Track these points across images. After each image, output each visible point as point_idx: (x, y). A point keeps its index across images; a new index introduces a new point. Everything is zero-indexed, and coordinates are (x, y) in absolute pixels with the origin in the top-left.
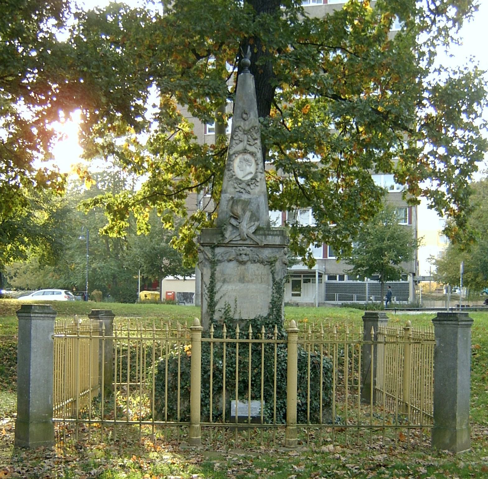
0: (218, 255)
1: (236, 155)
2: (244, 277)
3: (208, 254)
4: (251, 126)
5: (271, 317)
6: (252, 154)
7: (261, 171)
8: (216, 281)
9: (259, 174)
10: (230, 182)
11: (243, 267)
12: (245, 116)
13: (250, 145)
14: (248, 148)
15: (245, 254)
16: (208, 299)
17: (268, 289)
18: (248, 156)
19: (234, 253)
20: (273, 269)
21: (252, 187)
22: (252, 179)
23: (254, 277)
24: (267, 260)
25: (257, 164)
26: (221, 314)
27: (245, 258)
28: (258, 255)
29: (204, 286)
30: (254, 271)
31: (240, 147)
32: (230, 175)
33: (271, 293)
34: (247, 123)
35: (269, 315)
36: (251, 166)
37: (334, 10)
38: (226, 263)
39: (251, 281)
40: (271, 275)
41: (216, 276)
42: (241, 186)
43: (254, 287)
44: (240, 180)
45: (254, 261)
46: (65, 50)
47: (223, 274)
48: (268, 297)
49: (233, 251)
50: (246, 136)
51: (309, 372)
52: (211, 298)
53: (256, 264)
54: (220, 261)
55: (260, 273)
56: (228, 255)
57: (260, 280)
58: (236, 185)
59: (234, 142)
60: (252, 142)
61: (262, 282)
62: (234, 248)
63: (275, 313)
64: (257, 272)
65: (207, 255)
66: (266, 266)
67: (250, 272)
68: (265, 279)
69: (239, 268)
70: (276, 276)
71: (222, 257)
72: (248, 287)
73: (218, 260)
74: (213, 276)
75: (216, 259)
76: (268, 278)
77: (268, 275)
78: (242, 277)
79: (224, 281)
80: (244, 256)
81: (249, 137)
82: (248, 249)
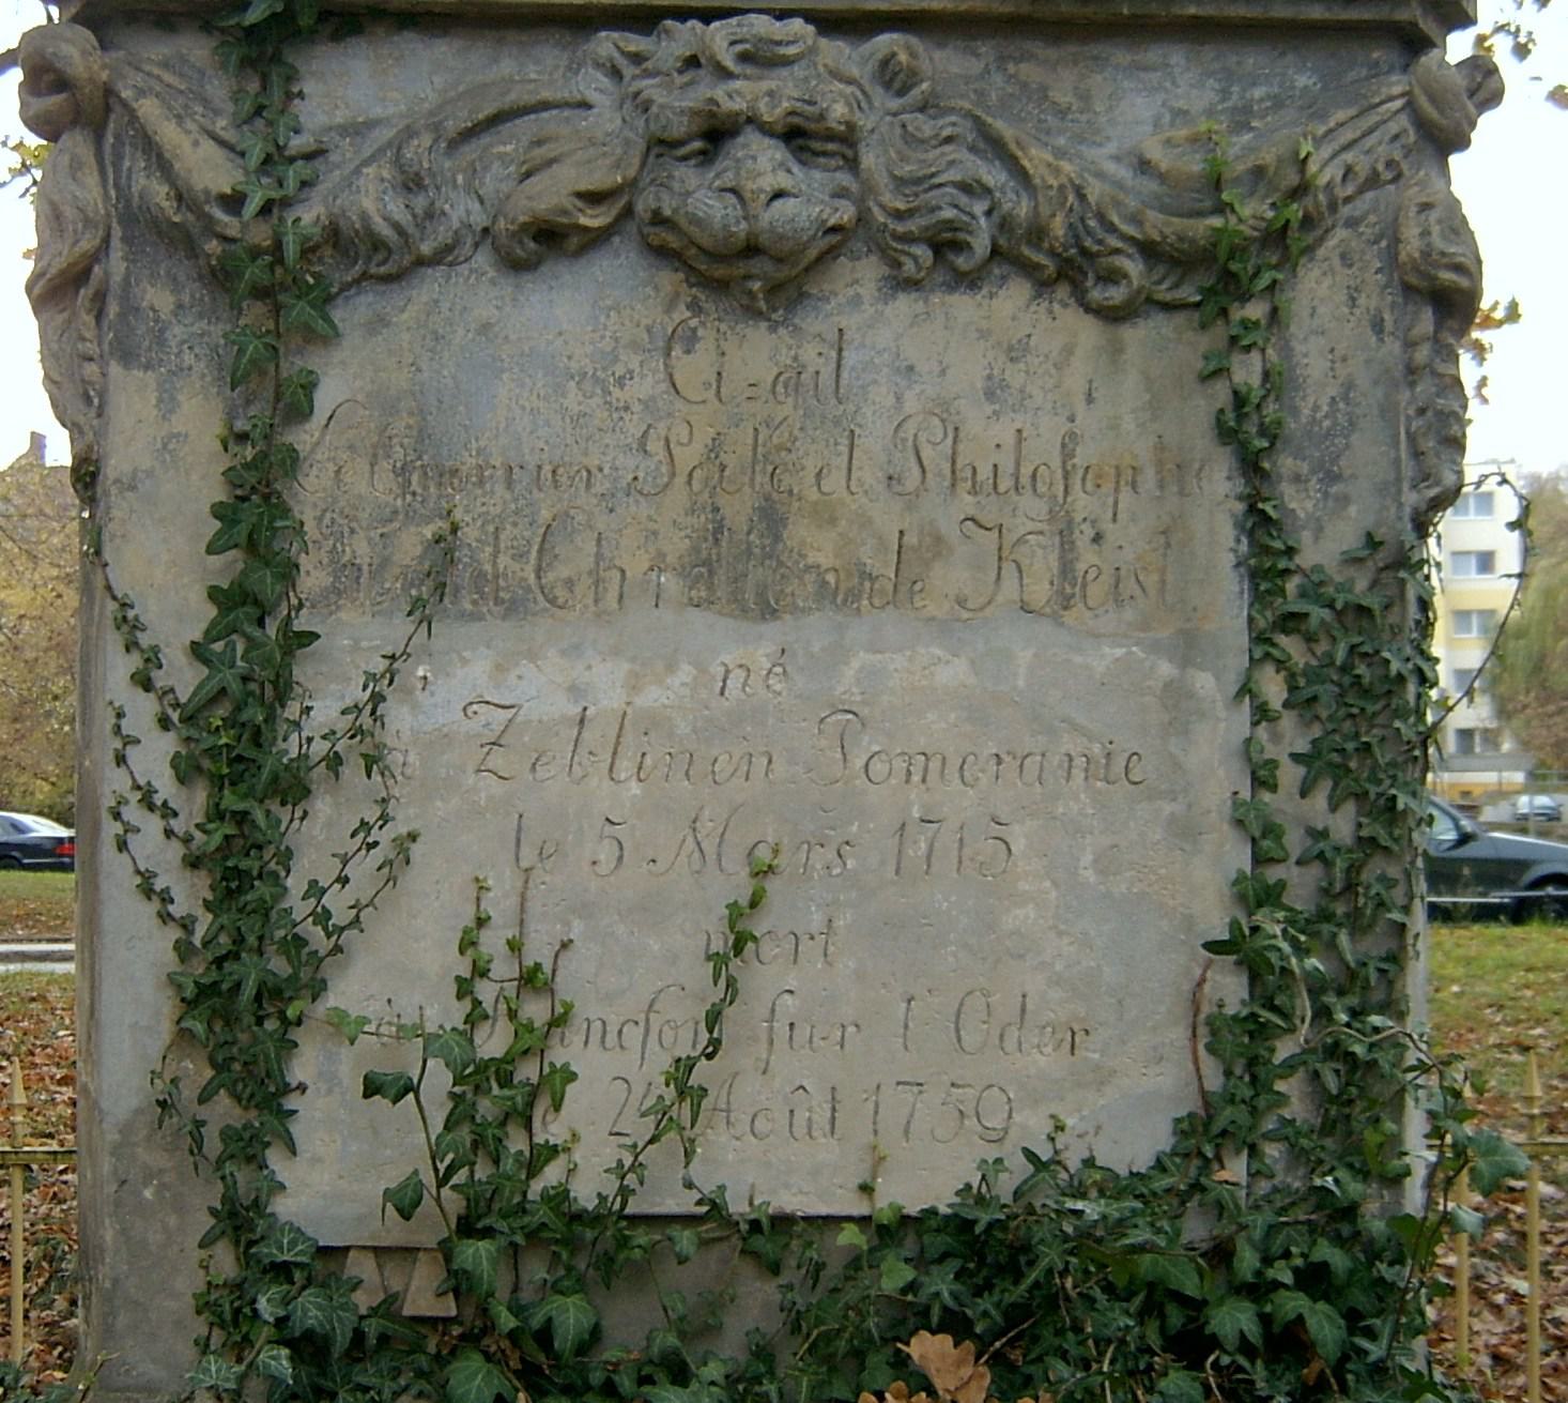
0: (344, 152)
2: (771, 518)
3: (169, 134)
5: (1236, 1169)
8: (313, 578)
11: (756, 352)
15: (798, 137)
16: (189, 893)
17: (1176, 696)
19: (607, 117)
20: (1247, 372)
23: (947, 514)
24: (1157, 225)
26: (405, 1142)
27: (789, 196)
28: (995, 147)
29: (119, 667)
30: (942, 409)
33: (1217, 780)
35: (1202, 1135)
37: (1091, 1150)
38: (474, 295)
39: (893, 582)
40: (1220, 484)
41: (309, 496)
43: (953, 672)
45: (945, 243)
46: (930, 233)
47: (425, 464)
48: (1185, 831)
49: (592, 84)
52: (239, 867)
53: (964, 306)
54: (376, 260)
55: (1044, 448)
56: (508, 144)
57: (1042, 563)
61: (1069, 588)
62: (606, 43)
63: (1295, 1100)
64: (988, 436)
65: (162, 165)
66: (1135, 335)
67: (874, 437)
68: (1130, 538)
69: (694, 367)
70: (1296, 500)
71: (411, 183)
72: (846, 682)
73: (335, 236)
74: (255, 512)
75: (310, 215)
76: (1169, 535)
77: (1177, 472)
78: (739, 509)
79: (439, 587)
80: (762, 162)
82: (836, 51)
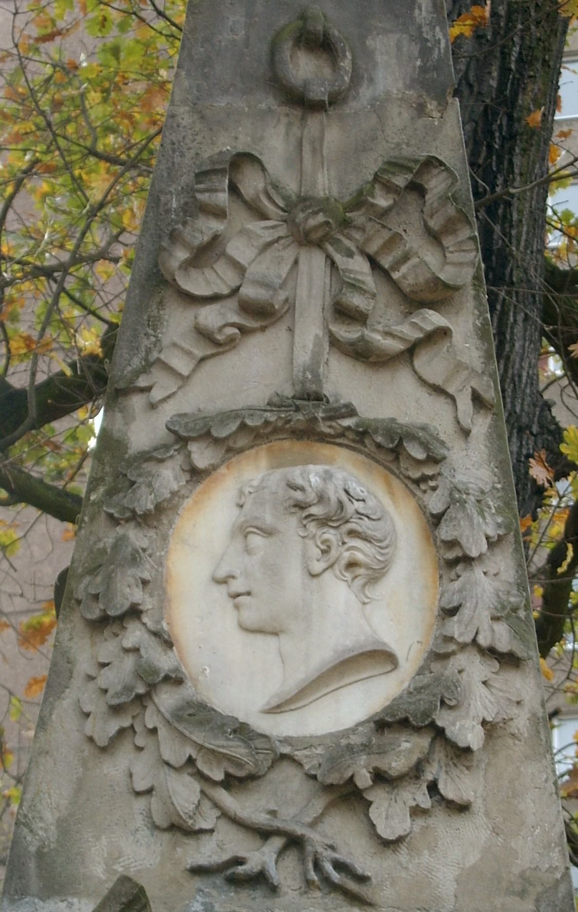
1: (202, 456)
4: (372, 164)
6: (393, 449)
7: (502, 637)
9: (474, 670)
10: (115, 768)
12: (304, 68)
13: (363, 355)
14: (345, 382)
18: (339, 473)
21: (390, 813)
22: (387, 724)
25: (455, 561)
31: (253, 374)
32: (122, 672)
34: (333, 134)
36: (376, 575)
42: (250, 806)
44: (242, 731)
50: (314, 264)
51: (524, 233)
58: (184, 793)
59: (177, 323)
60: (389, 328)
81: (359, 266)
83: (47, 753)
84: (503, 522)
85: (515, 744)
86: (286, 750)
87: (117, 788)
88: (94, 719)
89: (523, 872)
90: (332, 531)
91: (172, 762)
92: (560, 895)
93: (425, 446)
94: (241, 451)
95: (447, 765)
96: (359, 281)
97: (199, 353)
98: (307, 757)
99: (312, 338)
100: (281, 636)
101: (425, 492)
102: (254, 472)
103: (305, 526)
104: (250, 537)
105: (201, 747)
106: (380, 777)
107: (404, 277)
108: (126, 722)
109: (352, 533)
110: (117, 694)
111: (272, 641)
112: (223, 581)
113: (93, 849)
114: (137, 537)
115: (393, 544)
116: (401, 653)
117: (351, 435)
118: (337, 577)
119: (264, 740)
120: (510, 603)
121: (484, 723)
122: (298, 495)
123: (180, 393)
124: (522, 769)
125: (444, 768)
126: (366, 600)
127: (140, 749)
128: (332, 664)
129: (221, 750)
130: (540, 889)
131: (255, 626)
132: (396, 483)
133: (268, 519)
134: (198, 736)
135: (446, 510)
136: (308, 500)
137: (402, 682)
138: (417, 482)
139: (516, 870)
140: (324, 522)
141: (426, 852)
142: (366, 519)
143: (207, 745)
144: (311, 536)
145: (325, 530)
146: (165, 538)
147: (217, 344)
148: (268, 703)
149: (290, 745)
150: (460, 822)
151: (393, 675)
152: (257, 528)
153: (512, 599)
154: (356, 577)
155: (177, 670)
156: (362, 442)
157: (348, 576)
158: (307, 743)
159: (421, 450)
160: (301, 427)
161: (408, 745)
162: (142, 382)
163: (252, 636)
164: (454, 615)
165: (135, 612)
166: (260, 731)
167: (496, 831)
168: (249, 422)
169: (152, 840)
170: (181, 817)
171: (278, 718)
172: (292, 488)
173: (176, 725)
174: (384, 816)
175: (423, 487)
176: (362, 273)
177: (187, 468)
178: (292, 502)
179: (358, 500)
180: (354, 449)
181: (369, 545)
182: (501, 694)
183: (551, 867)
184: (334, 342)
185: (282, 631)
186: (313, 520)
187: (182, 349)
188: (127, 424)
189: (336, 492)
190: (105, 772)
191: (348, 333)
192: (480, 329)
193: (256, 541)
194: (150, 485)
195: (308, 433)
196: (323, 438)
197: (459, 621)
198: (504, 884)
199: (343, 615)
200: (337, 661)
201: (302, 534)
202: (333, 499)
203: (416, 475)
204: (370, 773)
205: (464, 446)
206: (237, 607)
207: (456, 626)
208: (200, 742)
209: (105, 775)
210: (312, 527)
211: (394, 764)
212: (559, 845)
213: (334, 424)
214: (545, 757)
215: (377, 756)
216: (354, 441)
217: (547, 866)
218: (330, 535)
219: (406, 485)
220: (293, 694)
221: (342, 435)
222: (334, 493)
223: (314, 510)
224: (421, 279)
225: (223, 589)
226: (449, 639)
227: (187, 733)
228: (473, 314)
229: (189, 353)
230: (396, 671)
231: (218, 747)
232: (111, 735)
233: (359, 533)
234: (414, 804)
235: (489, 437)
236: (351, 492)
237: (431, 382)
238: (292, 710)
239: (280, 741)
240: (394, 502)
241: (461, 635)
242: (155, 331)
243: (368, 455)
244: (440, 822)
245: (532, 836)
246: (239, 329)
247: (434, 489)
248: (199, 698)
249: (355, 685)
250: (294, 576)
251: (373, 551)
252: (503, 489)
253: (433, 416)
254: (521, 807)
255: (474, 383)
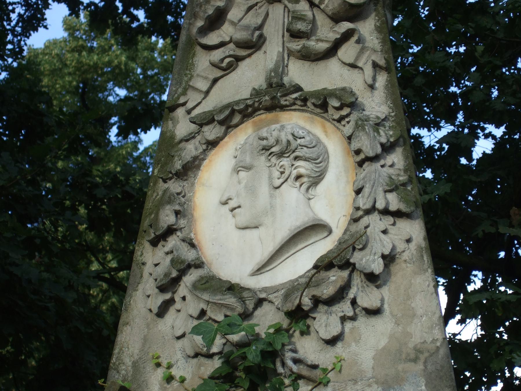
9: (376, 223)
13: (309, 57)
14: (299, 74)
36: (316, 180)
44: (232, 288)
83: (127, 324)
84: (393, 134)
85: (407, 267)
86: (263, 295)
87: (166, 338)
88: (152, 298)
89: (416, 345)
90: (285, 159)
91: (193, 315)
92: (440, 356)
93: (339, 98)
94: (236, 126)
95: (363, 287)
96: (302, 15)
97: (212, 77)
98: (275, 297)
99: (276, 53)
100: (260, 228)
101: (344, 126)
102: (244, 135)
103: (270, 160)
104: (240, 173)
105: (208, 302)
106: (317, 301)
107: (327, 6)
108: (168, 296)
109: (296, 158)
110: (161, 280)
111: (255, 232)
112: (225, 203)
113: (153, 377)
114: (174, 186)
115: (326, 159)
116: (333, 224)
117: (299, 102)
118: (291, 186)
119: (247, 292)
120: (400, 181)
121: (383, 257)
122: (265, 142)
123: (204, 102)
124: (413, 281)
125: (360, 289)
126: (311, 197)
127: (179, 311)
128: (288, 238)
129: (220, 302)
130: (426, 354)
131: (244, 225)
132: (328, 124)
133: (248, 160)
134: (206, 296)
135: (353, 133)
136: (270, 144)
137: (334, 242)
138: (339, 120)
139: (411, 345)
140: (281, 155)
141: (353, 344)
142: (305, 148)
143: (211, 300)
144: (273, 165)
145: (282, 159)
146: (193, 184)
147: (224, 69)
148: (252, 270)
149: (266, 292)
150: (374, 320)
151: (328, 238)
152: (242, 167)
153: (401, 178)
154: (302, 184)
155: (198, 259)
156: (305, 105)
157: (298, 184)
158: (275, 289)
159: (337, 101)
160: (268, 104)
161: (334, 278)
162: (182, 100)
163: (241, 231)
164: (360, 194)
165: (170, 231)
166: (247, 287)
167: (397, 324)
168: (236, 108)
169: (186, 365)
170: (199, 347)
171: (260, 277)
172: (261, 139)
173: (194, 292)
174: (324, 325)
175: (343, 123)
176: (304, 11)
177: (204, 142)
178: (261, 148)
179: (300, 138)
180: (303, 111)
181: (308, 163)
182: (396, 237)
183: (434, 339)
184: (291, 53)
185: (260, 225)
186: (274, 155)
187: (202, 77)
188: (174, 126)
189: (286, 135)
190: (160, 329)
191: (296, 45)
192: (379, 27)
193: (242, 174)
194: (180, 155)
195: (274, 107)
196: (283, 108)
197: (363, 197)
198: (404, 356)
199: (292, 208)
200: (291, 235)
201: (268, 165)
202: (284, 141)
203: (337, 116)
204: (311, 299)
205: (370, 95)
206: (234, 216)
207: (361, 200)
208: (207, 299)
209: (160, 331)
210: (274, 160)
211: (325, 291)
212: (438, 325)
213: (287, 98)
214: (427, 271)
215: (314, 288)
216: (301, 106)
217: (431, 339)
218: (285, 162)
219: (334, 125)
220: (266, 260)
221: (294, 104)
222: (284, 137)
223: (273, 150)
224: (336, 5)
225: (227, 207)
226: (358, 209)
227: (199, 295)
228: (375, 19)
229: (206, 78)
230: (332, 234)
231: (218, 300)
232: (159, 305)
233: (301, 157)
234: (342, 314)
235: (386, 87)
236: (296, 134)
237: (348, 62)
238: (268, 271)
239: (260, 291)
240: (327, 136)
241: (364, 204)
242: (190, 71)
243: (311, 112)
244: (362, 321)
245: (420, 322)
246: (234, 58)
247: (348, 122)
248: (211, 274)
249: (306, 248)
250: (264, 189)
251: (311, 166)
252: (395, 115)
253: (355, 82)
254: (413, 305)
255: (374, 57)
